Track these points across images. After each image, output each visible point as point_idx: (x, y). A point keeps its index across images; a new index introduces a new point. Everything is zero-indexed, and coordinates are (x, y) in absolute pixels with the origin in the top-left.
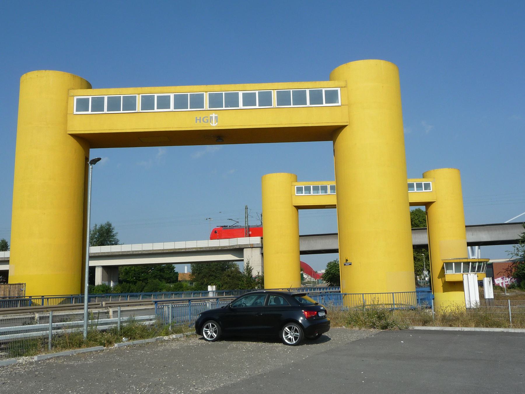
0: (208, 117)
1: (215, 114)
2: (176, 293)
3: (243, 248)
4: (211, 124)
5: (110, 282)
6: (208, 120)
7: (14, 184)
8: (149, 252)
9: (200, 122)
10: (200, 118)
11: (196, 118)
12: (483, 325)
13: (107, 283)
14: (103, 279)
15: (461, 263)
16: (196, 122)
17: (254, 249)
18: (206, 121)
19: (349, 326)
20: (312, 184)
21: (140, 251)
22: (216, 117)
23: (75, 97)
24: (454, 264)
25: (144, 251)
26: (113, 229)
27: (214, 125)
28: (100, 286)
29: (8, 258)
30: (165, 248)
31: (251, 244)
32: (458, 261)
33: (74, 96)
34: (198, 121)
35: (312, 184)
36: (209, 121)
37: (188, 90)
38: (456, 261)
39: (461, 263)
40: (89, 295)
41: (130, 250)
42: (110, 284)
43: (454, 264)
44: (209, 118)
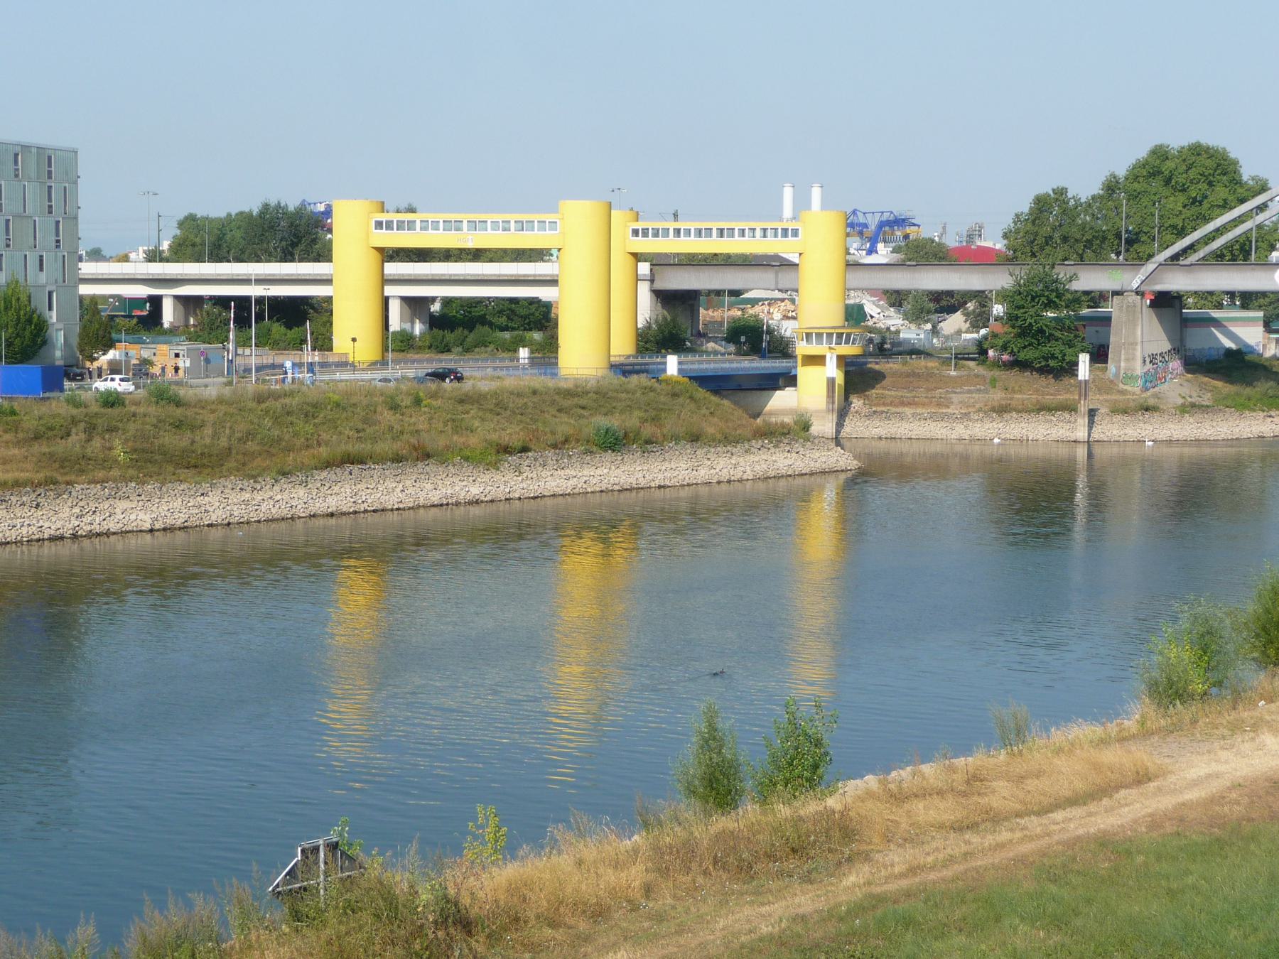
2: (936, 296)
5: (413, 323)
8: (477, 278)
13: (407, 326)
14: (402, 320)
15: (833, 334)
20: (441, 217)
21: (462, 275)
25: (468, 275)
26: (1003, 288)
28: (398, 332)
32: (821, 331)
35: (441, 217)
37: (499, 218)
39: (833, 334)
42: (413, 327)
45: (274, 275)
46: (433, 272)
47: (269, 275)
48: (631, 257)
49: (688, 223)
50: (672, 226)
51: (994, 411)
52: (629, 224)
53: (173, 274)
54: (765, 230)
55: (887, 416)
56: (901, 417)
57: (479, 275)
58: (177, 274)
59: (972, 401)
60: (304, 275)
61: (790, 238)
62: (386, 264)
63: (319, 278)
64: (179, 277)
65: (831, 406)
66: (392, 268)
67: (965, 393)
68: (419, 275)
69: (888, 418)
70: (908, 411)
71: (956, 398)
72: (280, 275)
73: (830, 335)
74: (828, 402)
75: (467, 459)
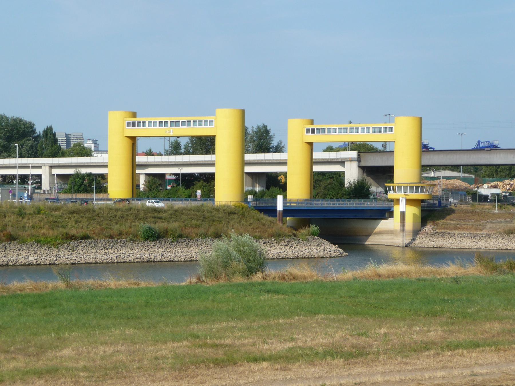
3: (345, 161)
17: (352, 162)
19: (219, 275)
21: (271, 160)
22: (172, 131)
24: (402, 187)
25: (274, 160)
29: (287, 160)
30: (72, 162)
31: (349, 158)
32: (400, 185)
38: (398, 185)
39: (414, 186)
40: (30, 175)
41: (264, 159)
43: (402, 187)
45: (186, 162)
46: (258, 159)
47: (185, 162)
48: (307, 145)
49: (335, 125)
50: (349, 126)
51: (505, 233)
52: (305, 126)
53: (142, 162)
54: (374, 128)
55: (442, 235)
56: (451, 236)
57: (278, 160)
58: (144, 162)
59: (498, 227)
60: (200, 161)
61: (388, 133)
62: (245, 154)
63: (206, 163)
64: (145, 164)
65: (402, 228)
66: (83, 141)
67: (497, 223)
68: (251, 160)
69: (442, 236)
70: (457, 232)
71: (489, 225)
72: (189, 161)
73: (405, 187)
74: (400, 226)
75: (38, 242)
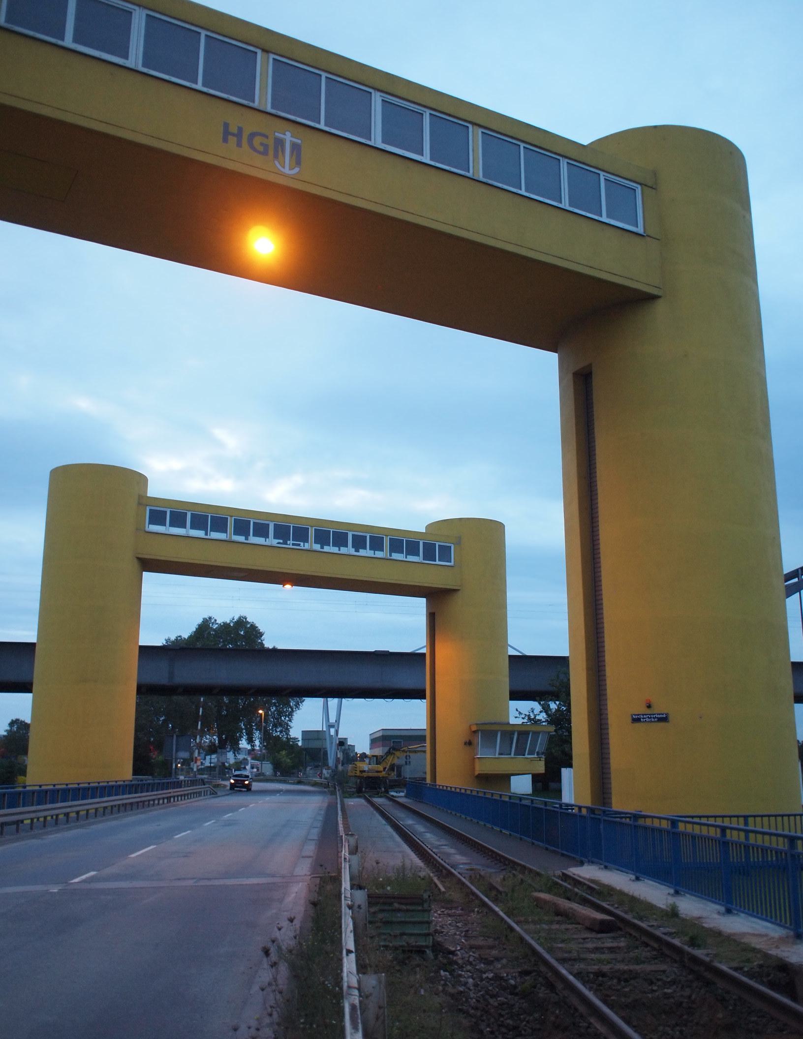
0: (267, 137)
1: (292, 136)
4: (276, 163)
6: (266, 147)
7: (562, 785)
9: (239, 144)
10: (240, 130)
11: (226, 126)
12: (367, 871)
16: (225, 140)
18: (261, 149)
23: (147, 507)
27: (287, 171)
33: (147, 505)
34: (232, 140)
36: (271, 152)
44: (271, 142)
